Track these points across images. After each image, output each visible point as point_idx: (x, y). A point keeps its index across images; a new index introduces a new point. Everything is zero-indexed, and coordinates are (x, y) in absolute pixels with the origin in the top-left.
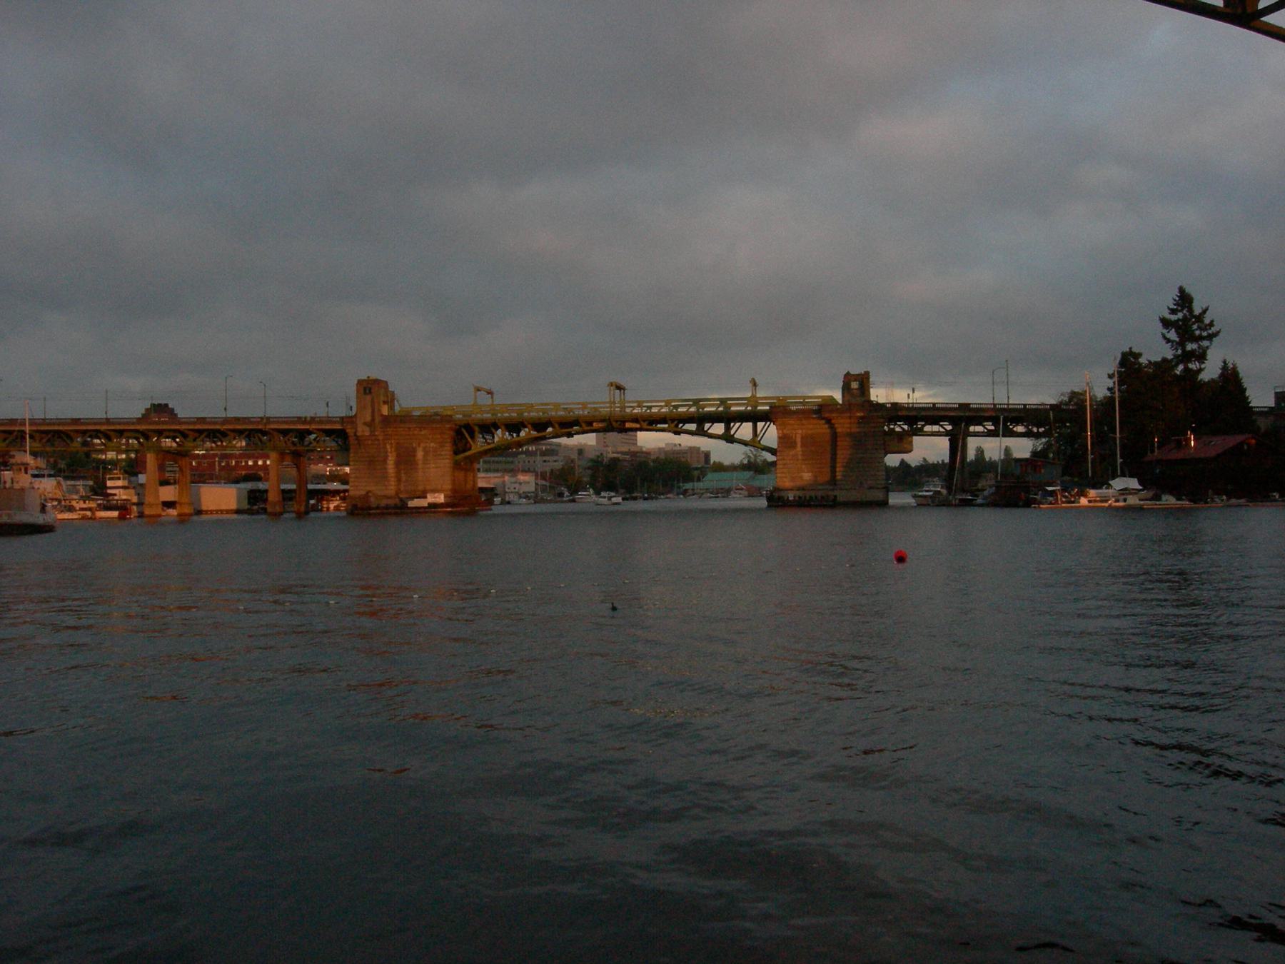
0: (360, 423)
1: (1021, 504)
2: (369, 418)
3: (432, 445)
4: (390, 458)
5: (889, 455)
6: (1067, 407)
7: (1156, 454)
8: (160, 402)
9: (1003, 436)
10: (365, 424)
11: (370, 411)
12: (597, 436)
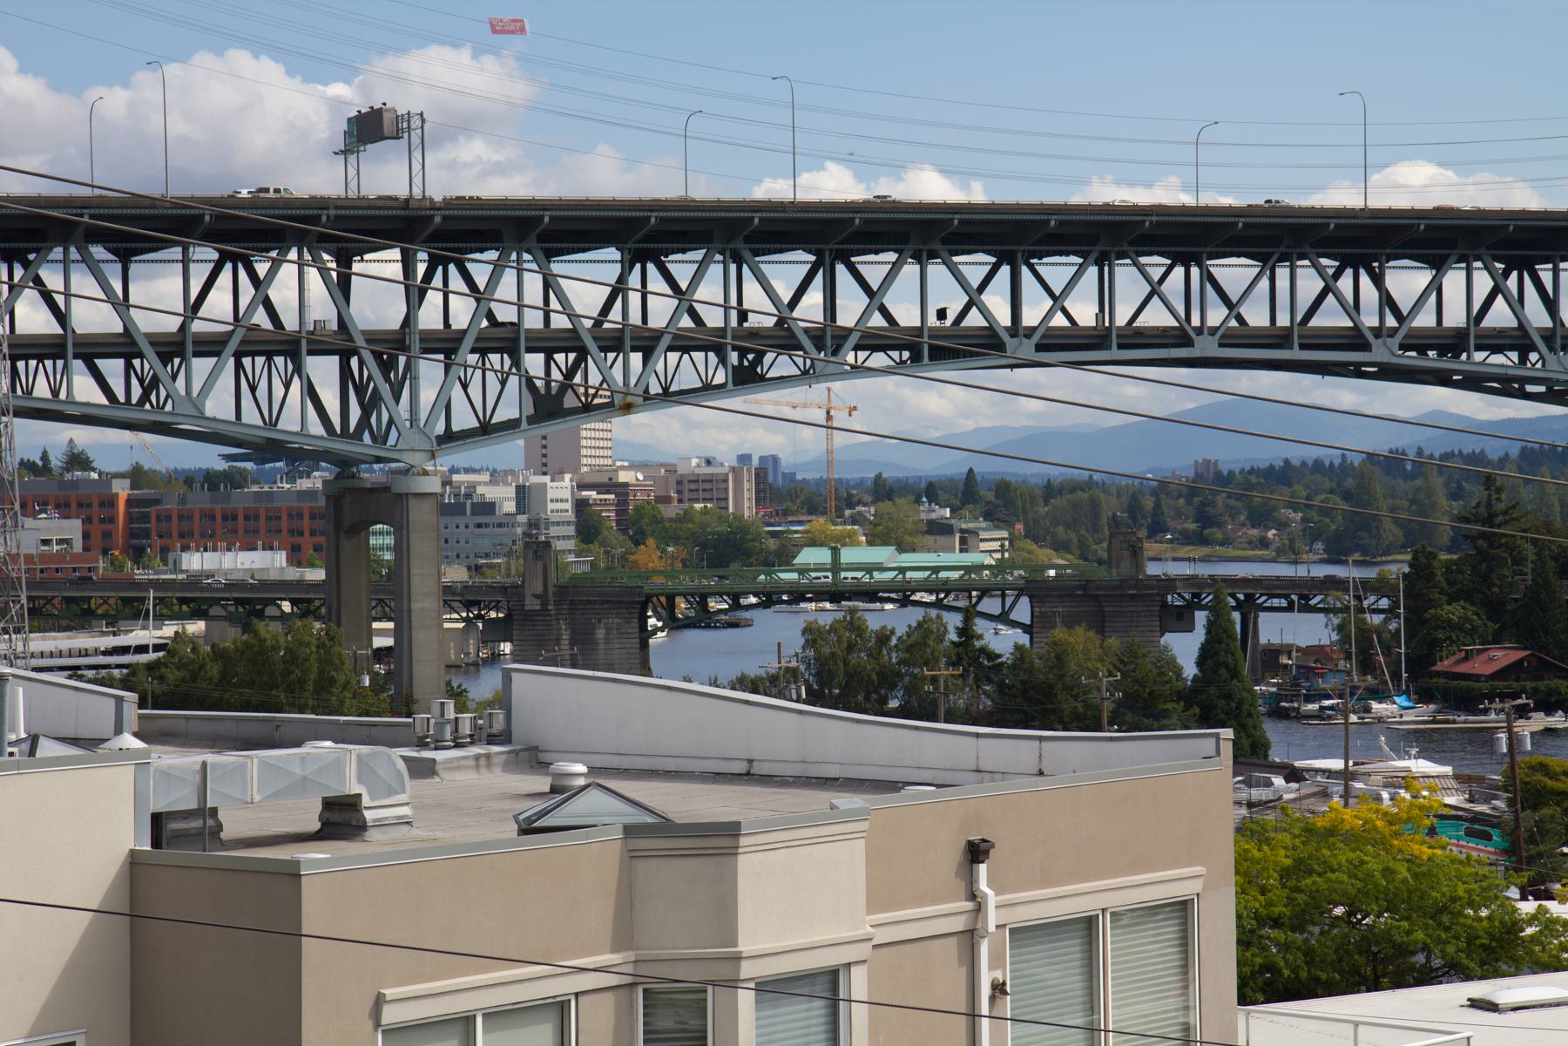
0: (528, 593)
1: (894, 704)
2: (539, 590)
3: (616, 620)
4: (564, 637)
5: (1167, 634)
6: (820, 605)
7: (170, 676)
8: (841, 476)
9: (1299, 611)
10: (536, 596)
11: (540, 580)
12: (377, 636)
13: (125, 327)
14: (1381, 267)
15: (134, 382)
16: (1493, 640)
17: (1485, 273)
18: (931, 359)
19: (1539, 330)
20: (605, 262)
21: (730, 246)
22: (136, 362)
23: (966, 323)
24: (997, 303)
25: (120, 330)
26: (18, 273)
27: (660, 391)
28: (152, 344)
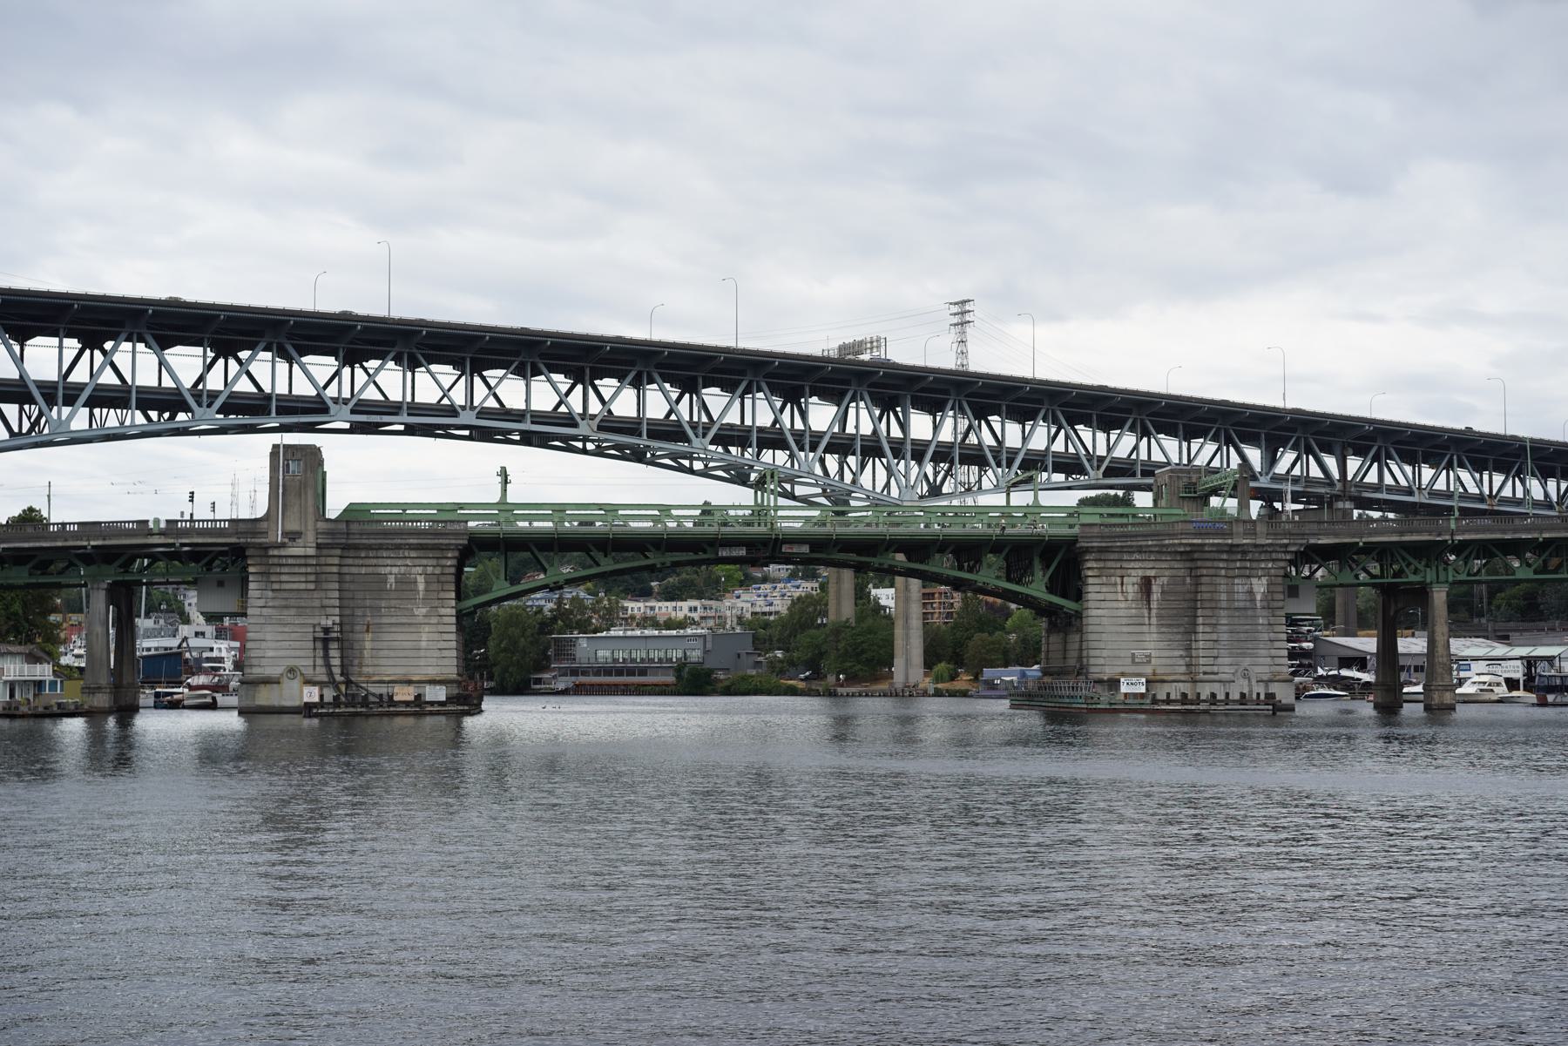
11: (510, 566)
13: (21, 376)
14: (806, 403)
15: (24, 418)
16: (1069, 578)
17: (866, 411)
18: (277, 414)
19: (989, 446)
20: (322, 366)
21: (137, 331)
22: (26, 407)
23: (442, 402)
24: (575, 401)
25: (17, 376)
26: (233, 366)
27: (118, 425)
28: (38, 387)
